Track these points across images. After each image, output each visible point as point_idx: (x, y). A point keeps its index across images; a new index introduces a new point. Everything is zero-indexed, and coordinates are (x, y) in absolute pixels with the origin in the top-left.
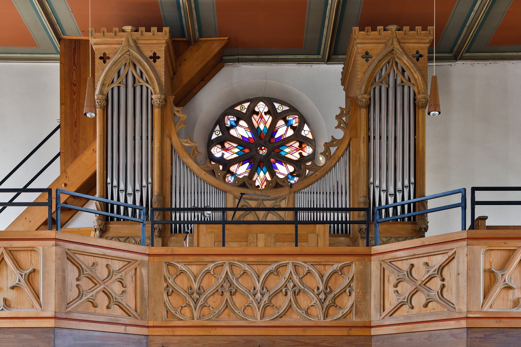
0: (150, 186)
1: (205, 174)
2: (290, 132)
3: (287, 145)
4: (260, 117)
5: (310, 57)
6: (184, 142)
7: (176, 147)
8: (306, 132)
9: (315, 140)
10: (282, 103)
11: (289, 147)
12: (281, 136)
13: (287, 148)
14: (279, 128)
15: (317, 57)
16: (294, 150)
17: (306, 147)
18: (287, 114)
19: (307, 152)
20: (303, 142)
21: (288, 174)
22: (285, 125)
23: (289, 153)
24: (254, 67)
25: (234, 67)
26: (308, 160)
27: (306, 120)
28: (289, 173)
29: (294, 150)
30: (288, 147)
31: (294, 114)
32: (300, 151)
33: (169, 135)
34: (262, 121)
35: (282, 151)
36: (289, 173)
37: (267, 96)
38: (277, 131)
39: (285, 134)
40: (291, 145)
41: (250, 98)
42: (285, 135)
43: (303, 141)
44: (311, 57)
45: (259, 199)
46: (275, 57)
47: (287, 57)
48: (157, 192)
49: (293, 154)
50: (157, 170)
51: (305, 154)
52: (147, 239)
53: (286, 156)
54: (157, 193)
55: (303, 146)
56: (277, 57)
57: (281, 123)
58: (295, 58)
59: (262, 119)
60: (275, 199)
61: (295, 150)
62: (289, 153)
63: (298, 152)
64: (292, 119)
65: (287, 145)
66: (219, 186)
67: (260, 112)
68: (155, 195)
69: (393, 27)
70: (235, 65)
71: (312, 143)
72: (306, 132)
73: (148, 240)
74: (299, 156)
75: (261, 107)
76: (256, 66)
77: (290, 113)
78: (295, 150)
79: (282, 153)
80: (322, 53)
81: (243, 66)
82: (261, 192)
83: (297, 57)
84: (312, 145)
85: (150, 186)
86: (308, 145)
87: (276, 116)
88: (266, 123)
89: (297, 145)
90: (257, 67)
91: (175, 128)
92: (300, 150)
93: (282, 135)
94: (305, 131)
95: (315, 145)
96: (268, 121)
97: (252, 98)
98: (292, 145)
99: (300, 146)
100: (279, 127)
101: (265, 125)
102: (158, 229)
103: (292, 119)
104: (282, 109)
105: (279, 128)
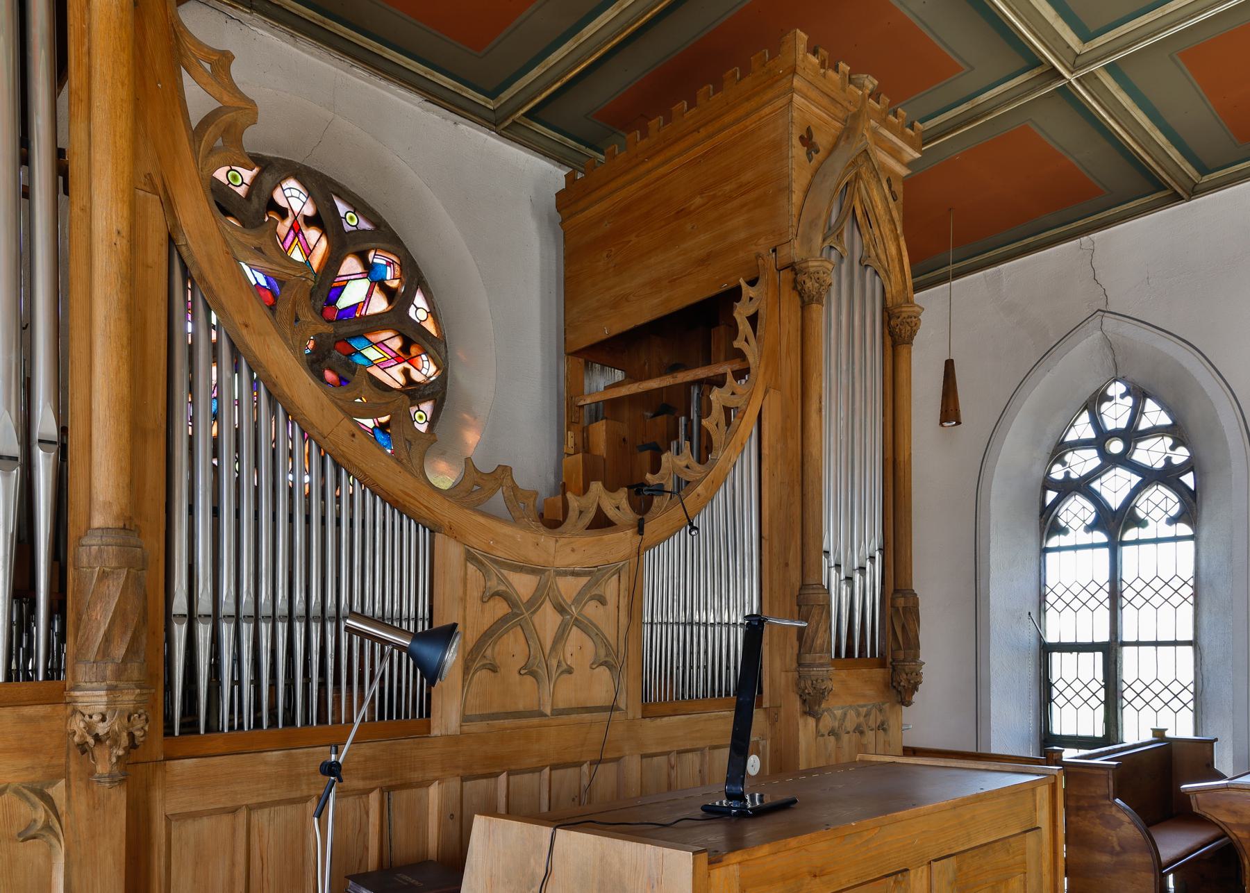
0: (43, 463)
1: (353, 435)
2: (379, 304)
3: (370, 337)
4: (292, 228)
5: (467, 92)
6: (244, 246)
7: (205, 266)
8: (419, 310)
9: (446, 343)
10: (359, 206)
11: (376, 344)
12: (354, 307)
13: (371, 346)
14: (348, 281)
15: (483, 103)
16: (390, 358)
17: (420, 355)
18: (373, 244)
19: (424, 371)
20: (413, 338)
21: (375, 427)
22: (366, 275)
23: (376, 364)
24: (295, 50)
25: (229, 21)
26: (429, 394)
27: (422, 277)
28: (378, 425)
29: (390, 358)
30: (374, 344)
31: (392, 250)
32: (406, 365)
33: (157, 181)
34: (299, 244)
35: (358, 352)
36: (378, 425)
37: (316, 169)
38: (342, 288)
39: (364, 302)
40: (382, 342)
41: (265, 154)
42: (365, 308)
43: (413, 338)
44: (470, 94)
45: (546, 571)
46: (374, 46)
47: (408, 64)
48: (116, 509)
49: (387, 370)
50: (118, 372)
51: (417, 376)
52: (28, 799)
53: (369, 370)
54: (117, 518)
55: (414, 350)
56: (380, 49)
57: (351, 265)
58: (429, 77)
59: (296, 235)
60: (592, 572)
61: (392, 358)
62: (376, 364)
63: (401, 366)
64: (384, 263)
65: (370, 337)
66: (408, 498)
67: (290, 213)
68: (98, 521)
69: (870, 82)
70: (236, 13)
71: (437, 347)
72: (419, 310)
73: (34, 806)
74: (401, 380)
75: (293, 196)
76: (303, 51)
77: (381, 245)
78: (392, 358)
79: (358, 360)
80: (506, 96)
81: (260, 31)
82: (557, 541)
83: (434, 76)
84: (440, 356)
85: (43, 463)
86: (426, 353)
87: (341, 244)
88: (311, 251)
89: (396, 344)
90: (307, 56)
91: (196, 153)
92: (407, 361)
93: (358, 304)
94: (417, 308)
95: (446, 356)
96: (315, 246)
97: (269, 155)
98: (387, 343)
99: (405, 348)
100: (349, 278)
101: (307, 257)
102: (124, 740)
103: (384, 263)
104: (355, 223)
105: (348, 281)
